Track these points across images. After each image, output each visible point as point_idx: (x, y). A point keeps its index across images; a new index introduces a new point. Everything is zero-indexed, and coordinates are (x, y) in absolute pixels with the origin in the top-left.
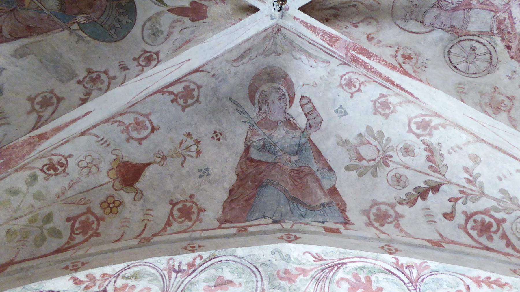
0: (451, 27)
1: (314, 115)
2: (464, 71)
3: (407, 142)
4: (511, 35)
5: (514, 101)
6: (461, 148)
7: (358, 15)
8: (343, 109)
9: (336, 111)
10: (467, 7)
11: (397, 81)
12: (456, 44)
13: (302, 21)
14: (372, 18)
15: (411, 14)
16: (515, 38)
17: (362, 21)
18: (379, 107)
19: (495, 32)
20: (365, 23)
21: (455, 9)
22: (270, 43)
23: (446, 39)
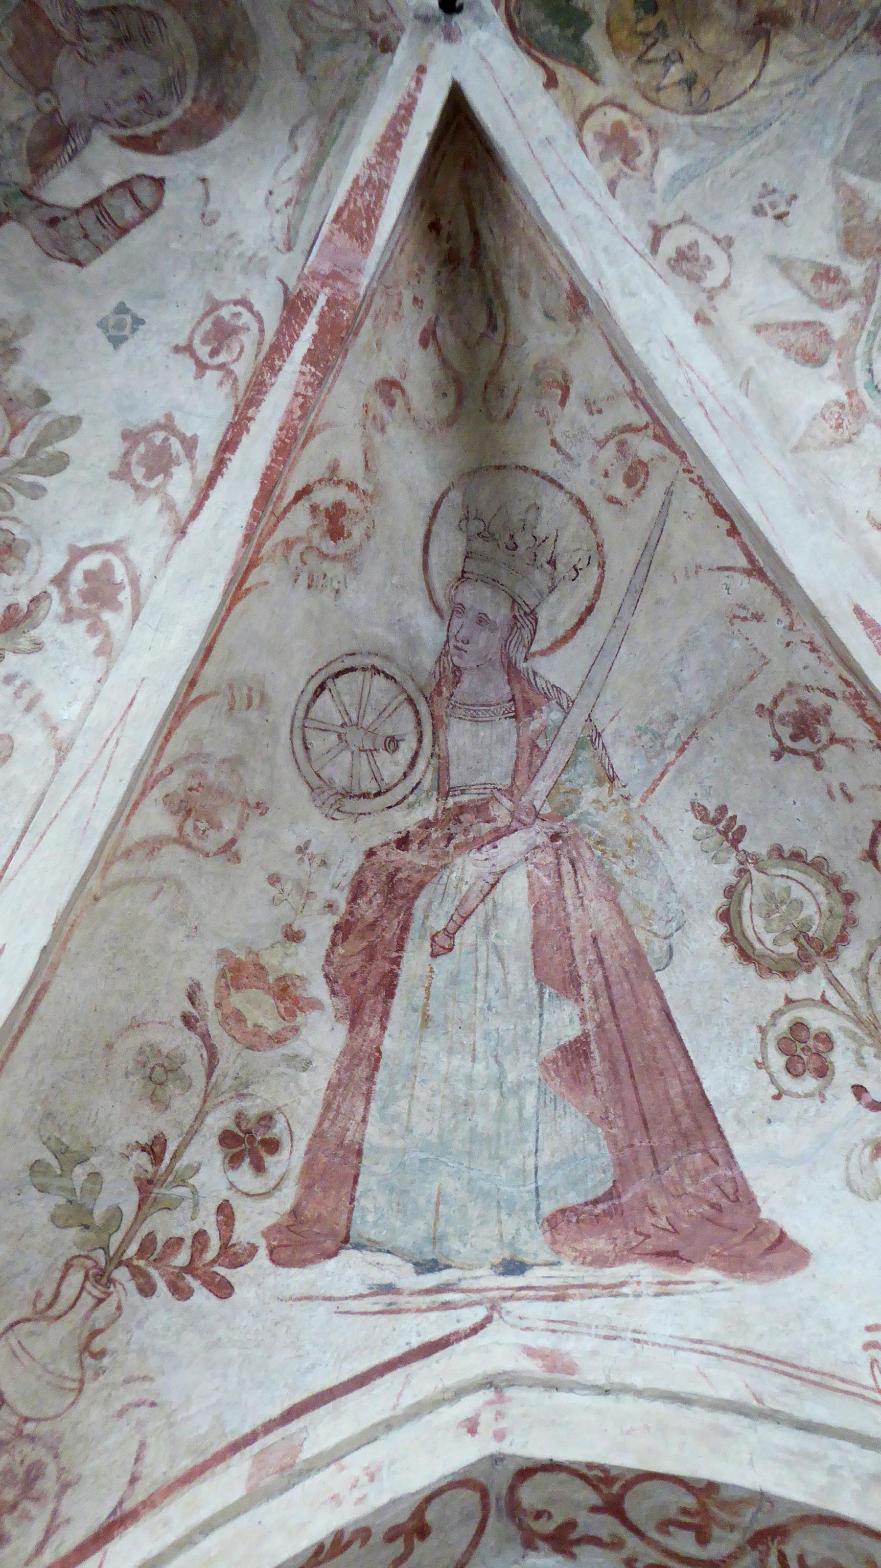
0: (457, 671)
1: (97, 233)
2: (311, 715)
3: (35, 548)
4: (442, 845)
5: (222, 858)
6: (28, 709)
7: (465, 343)
8: (134, 330)
9: (122, 309)
10: (520, 705)
11: (236, 461)
12: (404, 691)
13: (415, 101)
14: (460, 400)
15: (486, 535)
16: (435, 856)
17: (444, 362)
18: (150, 443)
19: (451, 802)
20: (438, 374)
21: (511, 669)
22: (336, 22)
23: (417, 659)
